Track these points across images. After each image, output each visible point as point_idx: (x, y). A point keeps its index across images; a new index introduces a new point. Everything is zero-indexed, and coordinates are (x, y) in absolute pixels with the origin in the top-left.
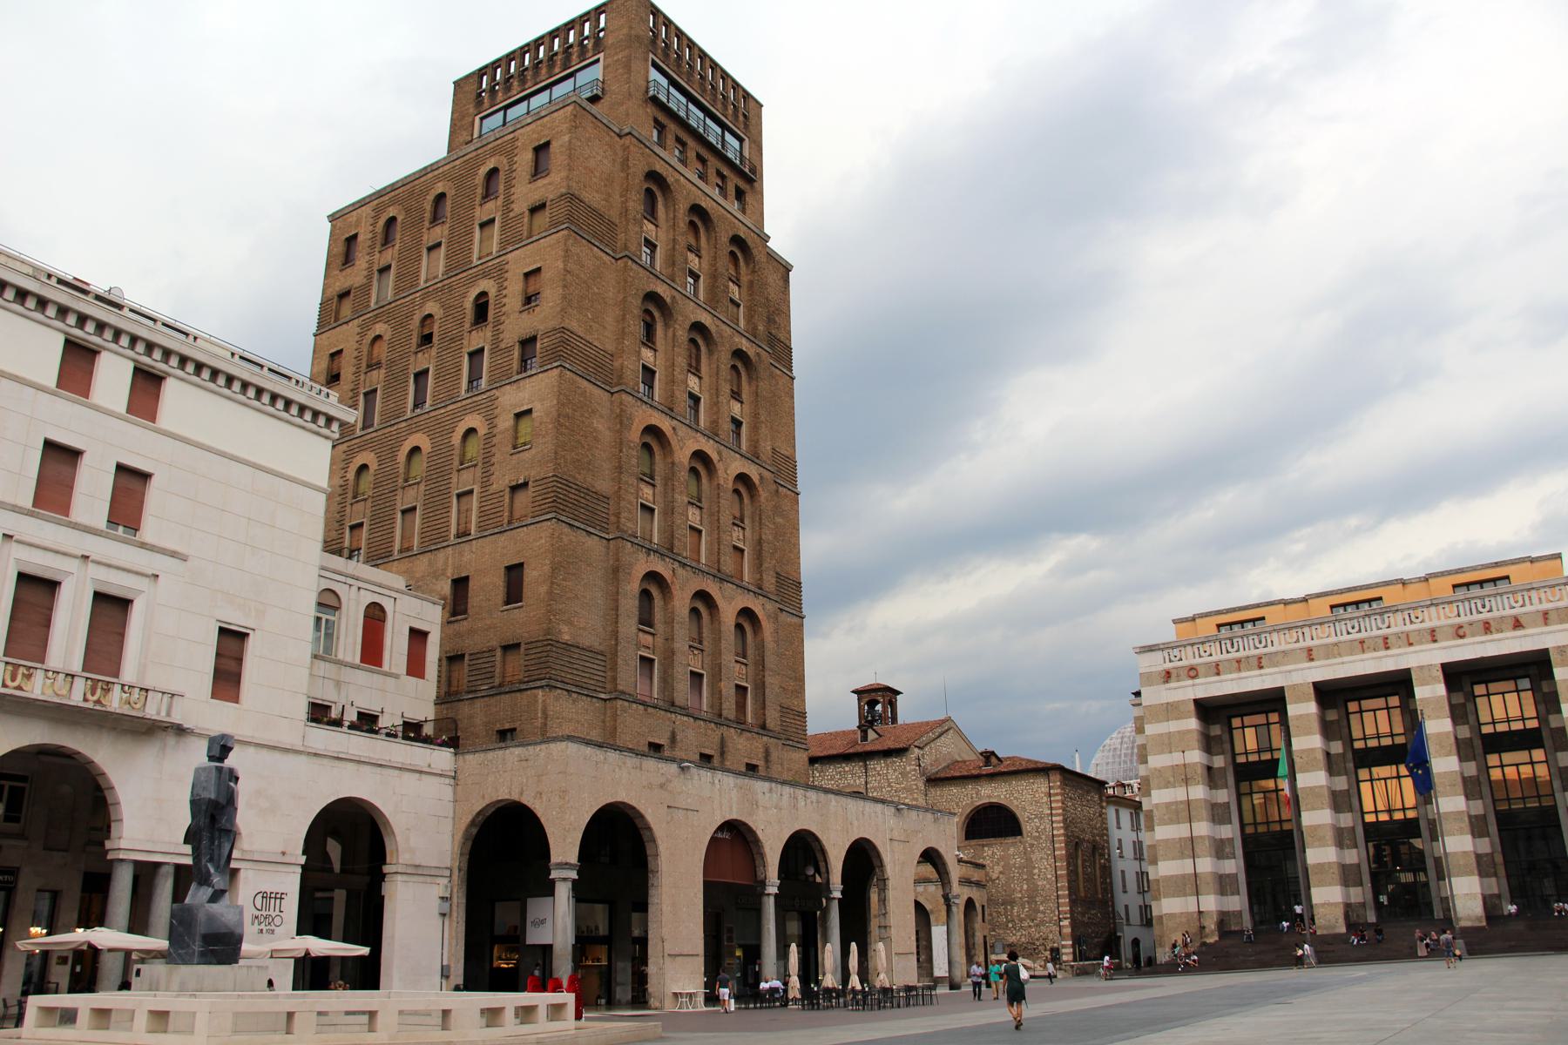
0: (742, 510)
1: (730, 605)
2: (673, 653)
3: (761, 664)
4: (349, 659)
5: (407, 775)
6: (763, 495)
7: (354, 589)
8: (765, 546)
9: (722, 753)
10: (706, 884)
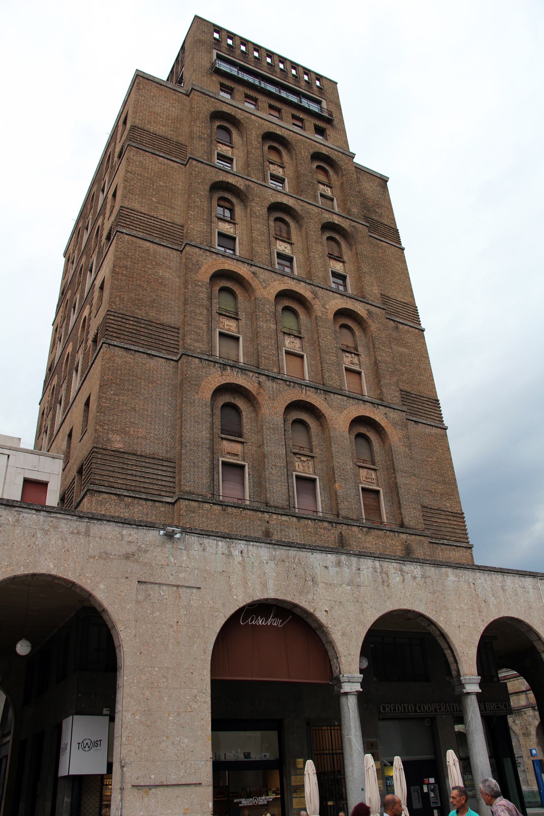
0: (355, 341)
2: (264, 456)
3: (392, 469)
6: (373, 327)
8: (382, 366)
10: (214, 683)
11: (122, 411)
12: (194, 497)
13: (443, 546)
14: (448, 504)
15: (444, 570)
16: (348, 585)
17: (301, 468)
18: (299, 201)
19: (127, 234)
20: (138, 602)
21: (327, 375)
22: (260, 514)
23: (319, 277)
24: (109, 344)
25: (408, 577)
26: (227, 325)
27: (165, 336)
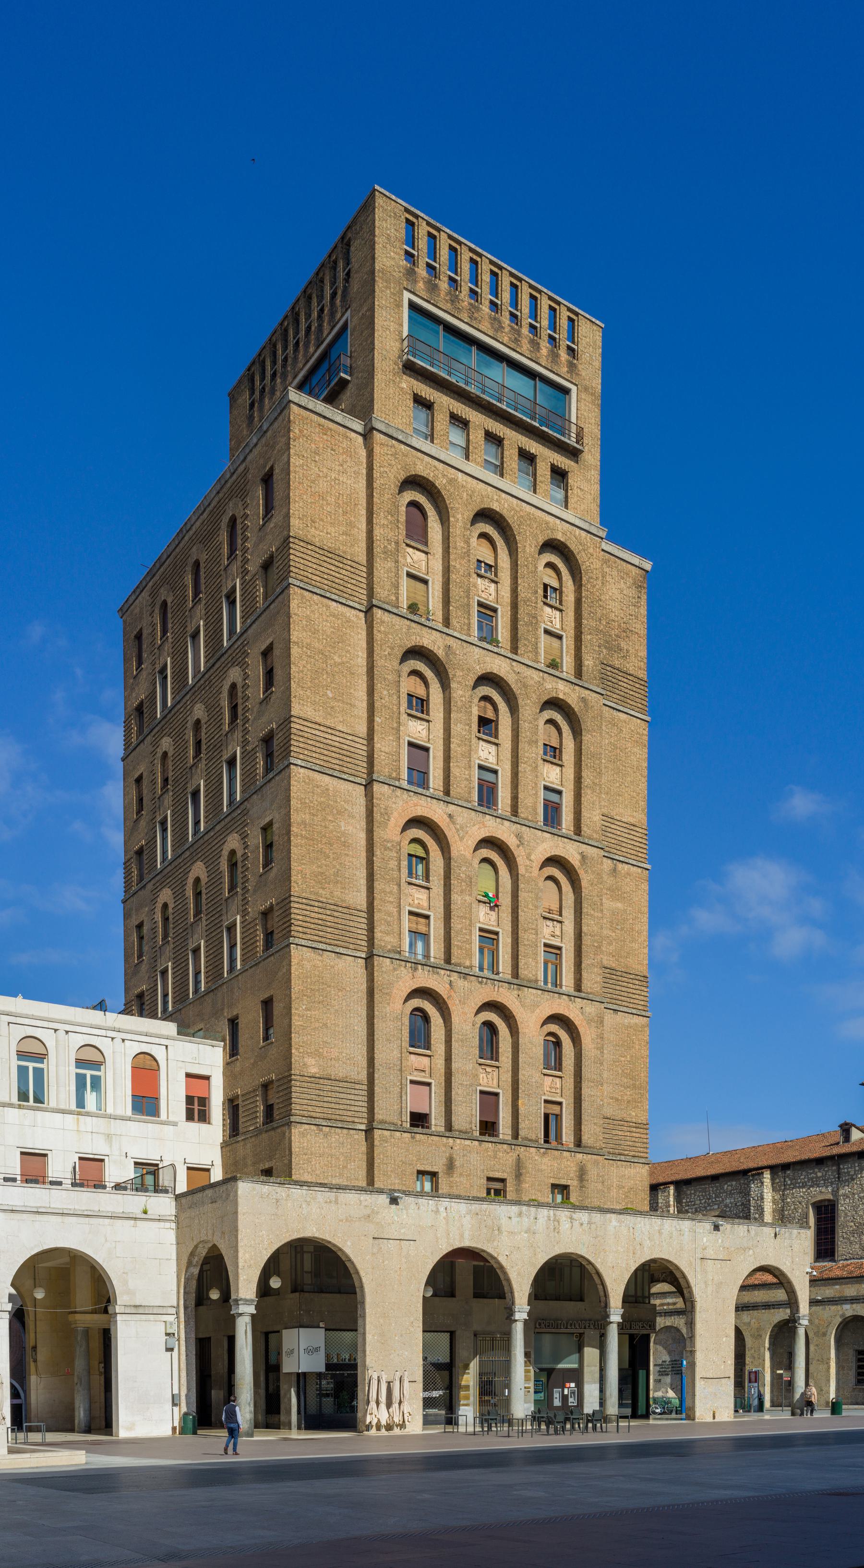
1: (531, 1013)
4: (120, 1112)
5: (119, 1222)
7: (118, 1041)
9: (518, 1176)
11: (315, 1029)
12: (387, 1126)
13: (619, 1163)
14: (634, 1114)
15: (609, 1216)
16: (526, 1232)
17: (485, 1080)
18: (514, 664)
19: (302, 767)
20: (373, 1254)
21: (523, 961)
22: (444, 1139)
23: (528, 807)
24: (297, 945)
25: (576, 1224)
26: (418, 898)
27: (351, 924)
